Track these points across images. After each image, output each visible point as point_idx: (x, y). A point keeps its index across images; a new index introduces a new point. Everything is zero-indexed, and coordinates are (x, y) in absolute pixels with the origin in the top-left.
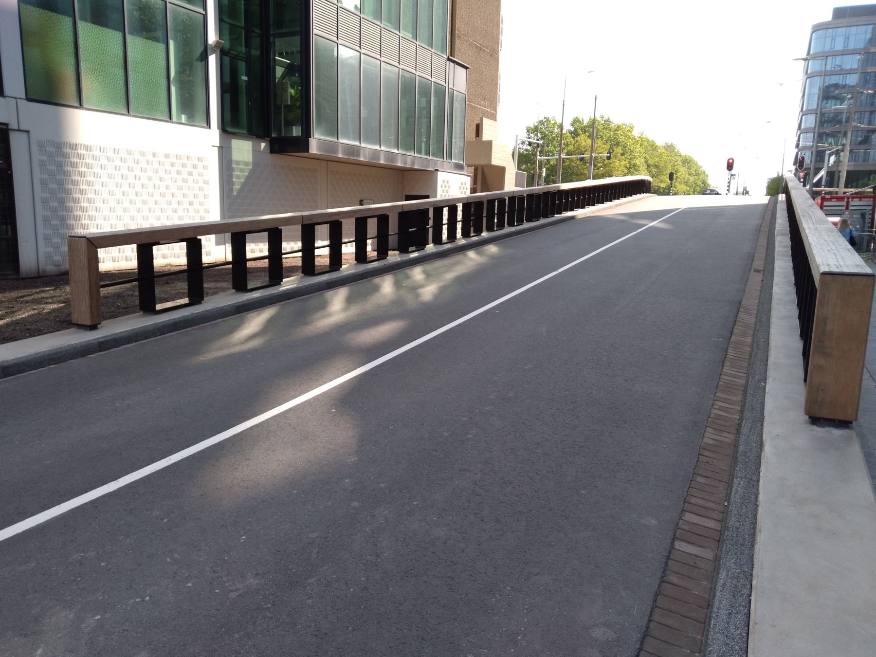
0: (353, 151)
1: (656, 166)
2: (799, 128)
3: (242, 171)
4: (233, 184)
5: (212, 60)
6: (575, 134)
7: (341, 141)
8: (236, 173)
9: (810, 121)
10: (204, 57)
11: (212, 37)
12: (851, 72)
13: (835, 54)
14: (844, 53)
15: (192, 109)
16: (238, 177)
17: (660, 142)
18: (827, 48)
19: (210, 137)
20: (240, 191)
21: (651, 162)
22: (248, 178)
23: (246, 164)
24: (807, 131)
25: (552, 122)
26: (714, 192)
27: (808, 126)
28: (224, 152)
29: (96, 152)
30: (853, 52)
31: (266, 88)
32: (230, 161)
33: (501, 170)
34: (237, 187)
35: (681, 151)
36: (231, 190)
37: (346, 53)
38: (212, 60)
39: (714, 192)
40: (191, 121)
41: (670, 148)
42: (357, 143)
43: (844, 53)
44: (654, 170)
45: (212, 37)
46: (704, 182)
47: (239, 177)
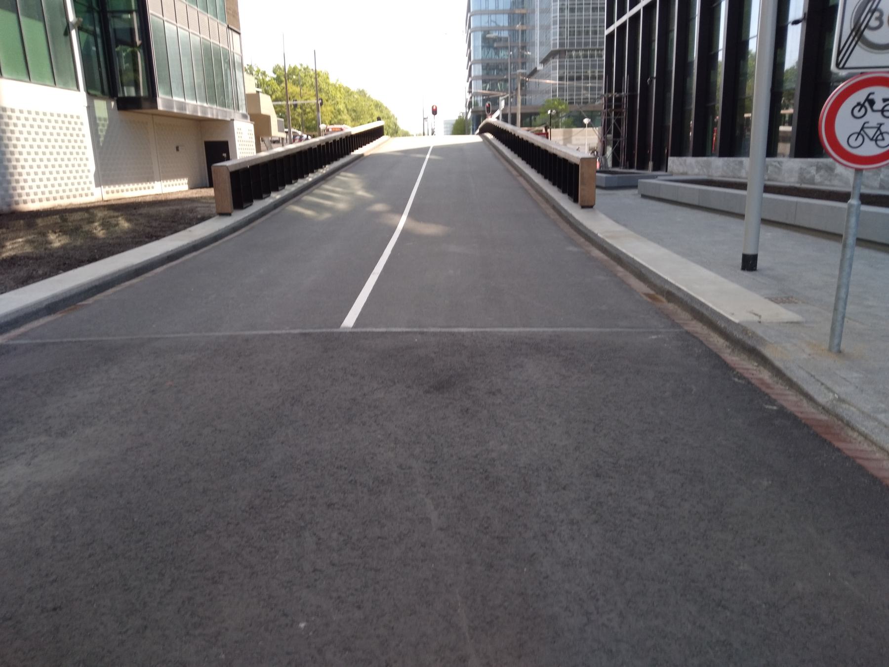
0: (182, 106)
1: (355, 111)
2: (470, 75)
3: (103, 125)
4: (99, 137)
5: (74, 33)
6: (278, 80)
7: (175, 98)
8: (100, 127)
9: (478, 70)
10: (67, 33)
11: (72, 17)
12: (503, 29)
13: (489, 13)
14: (497, 12)
15: (57, 75)
16: (102, 131)
17: (354, 88)
18: (483, 7)
19: (81, 96)
20: (104, 142)
21: (350, 107)
22: (107, 131)
23: (105, 120)
24: (476, 78)
25: (255, 69)
26: (406, 134)
27: (477, 74)
28: (91, 109)
29: (9, 113)
30: (503, 12)
31: (116, 58)
32: (95, 118)
33: (268, 118)
34: (102, 139)
35: (372, 97)
36: (99, 142)
37: (170, 28)
38: (74, 33)
39: (406, 134)
40: (66, 86)
41: (362, 93)
42: (183, 100)
43: (497, 12)
44: (353, 114)
45: (72, 17)
46: (396, 125)
47: (102, 129)
